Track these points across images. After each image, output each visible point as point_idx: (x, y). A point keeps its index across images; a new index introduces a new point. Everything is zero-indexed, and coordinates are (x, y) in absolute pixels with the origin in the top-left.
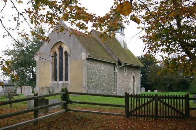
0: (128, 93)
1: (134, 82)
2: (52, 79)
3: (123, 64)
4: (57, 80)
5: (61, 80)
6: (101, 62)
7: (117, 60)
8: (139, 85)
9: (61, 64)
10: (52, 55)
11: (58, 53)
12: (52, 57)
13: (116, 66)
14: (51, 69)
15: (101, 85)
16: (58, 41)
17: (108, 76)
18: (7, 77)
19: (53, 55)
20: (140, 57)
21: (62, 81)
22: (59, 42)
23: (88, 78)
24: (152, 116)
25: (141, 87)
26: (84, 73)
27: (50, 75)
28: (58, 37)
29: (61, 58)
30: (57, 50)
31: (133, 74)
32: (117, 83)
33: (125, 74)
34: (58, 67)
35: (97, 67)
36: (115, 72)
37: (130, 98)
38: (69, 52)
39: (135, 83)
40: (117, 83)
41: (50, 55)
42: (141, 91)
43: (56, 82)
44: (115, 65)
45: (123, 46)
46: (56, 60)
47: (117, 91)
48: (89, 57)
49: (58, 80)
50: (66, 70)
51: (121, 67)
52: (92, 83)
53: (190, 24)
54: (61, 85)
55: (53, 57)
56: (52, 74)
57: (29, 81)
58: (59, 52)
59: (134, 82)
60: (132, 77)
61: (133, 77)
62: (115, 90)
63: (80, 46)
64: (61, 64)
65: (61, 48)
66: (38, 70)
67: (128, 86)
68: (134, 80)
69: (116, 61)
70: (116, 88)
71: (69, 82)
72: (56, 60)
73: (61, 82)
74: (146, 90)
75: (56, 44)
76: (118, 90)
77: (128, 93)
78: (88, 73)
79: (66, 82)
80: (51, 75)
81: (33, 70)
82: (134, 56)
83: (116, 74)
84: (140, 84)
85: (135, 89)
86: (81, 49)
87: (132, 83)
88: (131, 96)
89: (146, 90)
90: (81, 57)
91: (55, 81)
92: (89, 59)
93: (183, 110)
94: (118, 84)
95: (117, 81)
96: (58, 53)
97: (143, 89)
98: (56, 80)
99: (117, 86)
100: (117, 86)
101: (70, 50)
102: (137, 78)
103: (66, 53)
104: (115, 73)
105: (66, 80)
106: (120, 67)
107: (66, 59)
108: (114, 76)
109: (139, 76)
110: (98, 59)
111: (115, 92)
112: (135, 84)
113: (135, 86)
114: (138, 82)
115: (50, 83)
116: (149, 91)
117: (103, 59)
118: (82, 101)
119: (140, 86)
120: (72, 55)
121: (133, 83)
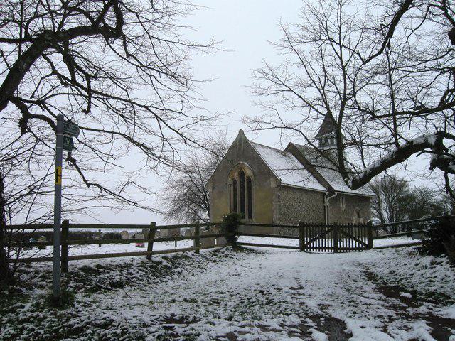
3: (336, 193)
9: (242, 194)
11: (238, 180)
18: (264, 278)
24: (331, 248)
29: (242, 187)
34: (238, 199)
37: (305, 228)
41: (227, 184)
46: (235, 190)
58: (240, 178)
64: (242, 194)
72: (235, 190)
78: (280, 206)
81: (328, 226)
88: (307, 226)
96: (238, 180)
101: (255, 176)
105: (250, 217)
107: (250, 188)
118: (271, 244)
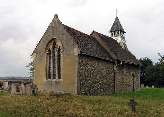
1: (134, 80)
3: (122, 62)
5: (54, 78)
6: (98, 59)
7: (116, 58)
8: (138, 82)
10: (47, 52)
12: (47, 54)
13: (116, 64)
14: (45, 65)
15: (97, 82)
17: (106, 74)
20: (140, 60)
22: (54, 38)
23: (82, 76)
25: (141, 83)
26: (77, 70)
27: (44, 73)
28: (53, 34)
30: (51, 47)
31: (133, 72)
32: (116, 80)
33: (125, 72)
36: (115, 70)
39: (135, 80)
40: (116, 80)
42: (140, 86)
43: (50, 80)
44: (114, 63)
45: (123, 47)
48: (82, 52)
50: (59, 67)
53: (158, 84)
54: (54, 82)
55: (48, 54)
59: (134, 80)
61: (133, 75)
62: (114, 87)
63: (72, 41)
65: (55, 45)
66: (35, 68)
67: (128, 83)
69: (114, 60)
70: (115, 86)
71: (61, 80)
73: (55, 80)
74: (145, 86)
80: (45, 72)
82: (137, 60)
83: (115, 72)
84: (139, 81)
85: (135, 86)
86: (74, 45)
87: (131, 80)
89: (145, 86)
90: (74, 53)
92: (81, 55)
93: (121, 32)
94: (117, 82)
95: (116, 78)
97: (143, 85)
99: (116, 83)
101: (63, 46)
102: (136, 76)
103: (59, 49)
104: (114, 71)
105: (59, 77)
109: (139, 75)
112: (135, 82)
113: (135, 83)
114: (137, 80)
115: (45, 80)
116: (147, 87)
119: (139, 83)
120: (64, 51)
121: (133, 81)
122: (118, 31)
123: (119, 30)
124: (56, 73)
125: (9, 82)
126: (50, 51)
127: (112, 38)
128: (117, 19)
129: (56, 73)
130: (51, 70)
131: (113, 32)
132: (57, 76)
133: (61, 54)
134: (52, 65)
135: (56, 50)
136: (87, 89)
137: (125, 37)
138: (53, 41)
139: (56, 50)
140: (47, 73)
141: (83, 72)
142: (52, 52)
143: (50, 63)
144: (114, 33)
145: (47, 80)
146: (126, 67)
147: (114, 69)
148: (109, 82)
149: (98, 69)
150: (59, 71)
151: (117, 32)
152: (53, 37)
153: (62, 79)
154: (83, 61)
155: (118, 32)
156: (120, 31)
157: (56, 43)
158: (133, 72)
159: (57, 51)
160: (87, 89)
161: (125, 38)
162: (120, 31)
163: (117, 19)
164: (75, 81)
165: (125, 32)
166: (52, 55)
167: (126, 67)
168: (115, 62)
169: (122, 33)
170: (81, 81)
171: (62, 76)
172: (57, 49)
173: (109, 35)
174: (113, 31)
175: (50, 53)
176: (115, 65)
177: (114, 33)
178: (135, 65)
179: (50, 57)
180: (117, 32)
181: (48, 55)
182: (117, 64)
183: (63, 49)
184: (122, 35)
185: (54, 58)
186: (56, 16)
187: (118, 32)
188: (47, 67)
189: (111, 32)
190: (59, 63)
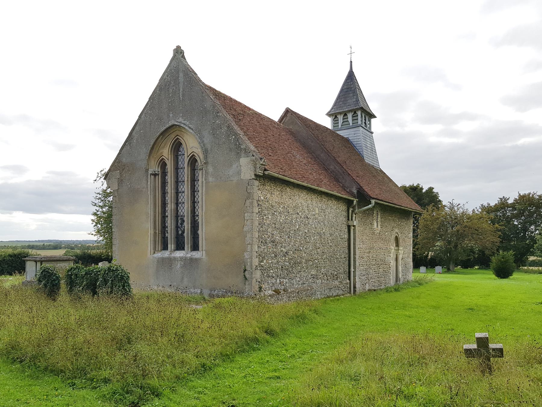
0: (420, 186)
2: (155, 241)
3: (373, 201)
4: (169, 246)
5: (180, 246)
10: (155, 168)
12: (155, 175)
16: (167, 126)
19: (158, 170)
21: (183, 249)
22: (173, 125)
30: (166, 152)
31: (397, 230)
35: (296, 207)
36: (350, 223)
38: (202, 156)
40: (355, 254)
41: (147, 170)
47: (355, 276)
49: (171, 246)
51: (368, 210)
52: (276, 256)
56: (155, 228)
57: (433, 253)
60: (393, 237)
65: (177, 147)
67: (384, 262)
68: (397, 245)
70: (352, 270)
73: (179, 254)
75: (163, 133)
76: (357, 273)
77: (420, 186)
79: (196, 255)
80: (151, 232)
85: (400, 268)
91: (196, 252)
94: (357, 257)
96: (170, 167)
98: (165, 248)
100: (355, 261)
101: (206, 152)
103: (193, 161)
105: (195, 247)
106: (364, 211)
108: (346, 236)
110: (295, 181)
111: (350, 279)
117: (318, 186)
120: (210, 169)
122: (355, 113)
123: (358, 109)
124: (188, 235)
125: (36, 262)
126: (163, 165)
127: (338, 132)
128: (351, 77)
129: (188, 235)
130: (168, 213)
131: (339, 116)
132: (188, 245)
133: (200, 176)
134: (170, 207)
135: (185, 162)
136: (278, 281)
137: (372, 130)
138: (173, 136)
139: (185, 162)
140: (155, 233)
141: (269, 230)
142: (170, 167)
143: (164, 204)
144: (340, 118)
145: (159, 255)
146: (379, 216)
147: (348, 220)
148: (337, 258)
149: (311, 221)
150: (195, 226)
151: (350, 116)
152: (170, 124)
153: (204, 252)
154: (269, 195)
155: (355, 116)
156: (359, 113)
157: (182, 142)
158: (397, 230)
159: (186, 165)
160: (278, 281)
161: (372, 133)
162: (359, 113)
163: (351, 77)
164: (246, 257)
165: (374, 117)
166: (170, 178)
167: (379, 216)
168: (353, 201)
169: (365, 120)
170: (264, 258)
171: (202, 242)
172: (186, 160)
173: (327, 123)
174: (340, 113)
175: (164, 174)
176: (351, 209)
177: (340, 118)
178: (404, 210)
179: (164, 183)
180: (350, 116)
181: (159, 179)
182: (358, 208)
183: (206, 157)
184: (365, 123)
185: (177, 188)
186: (179, 52)
187: (355, 116)
188: (155, 216)
189: (333, 115)
190: (194, 203)
